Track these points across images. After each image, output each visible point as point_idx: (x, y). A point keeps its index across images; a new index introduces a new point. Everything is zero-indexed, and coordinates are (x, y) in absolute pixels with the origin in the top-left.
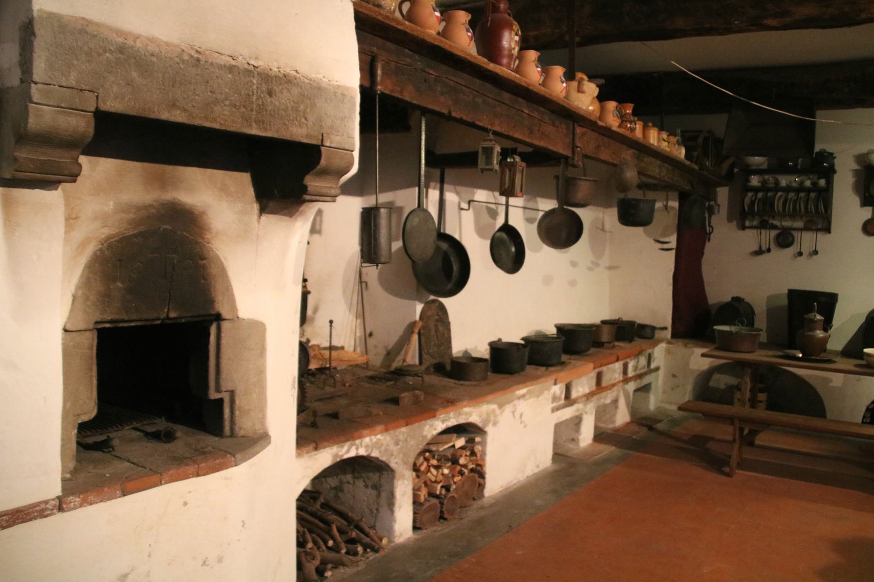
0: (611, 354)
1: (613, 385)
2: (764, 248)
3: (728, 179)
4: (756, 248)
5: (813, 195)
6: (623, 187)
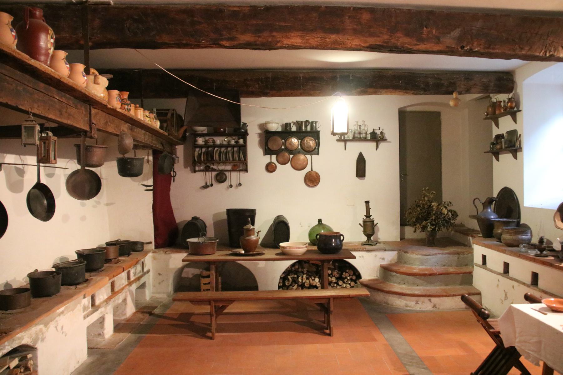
0: (118, 267)
1: (123, 289)
2: (208, 184)
3: (184, 140)
4: (204, 184)
5: (236, 149)
6: (123, 150)
